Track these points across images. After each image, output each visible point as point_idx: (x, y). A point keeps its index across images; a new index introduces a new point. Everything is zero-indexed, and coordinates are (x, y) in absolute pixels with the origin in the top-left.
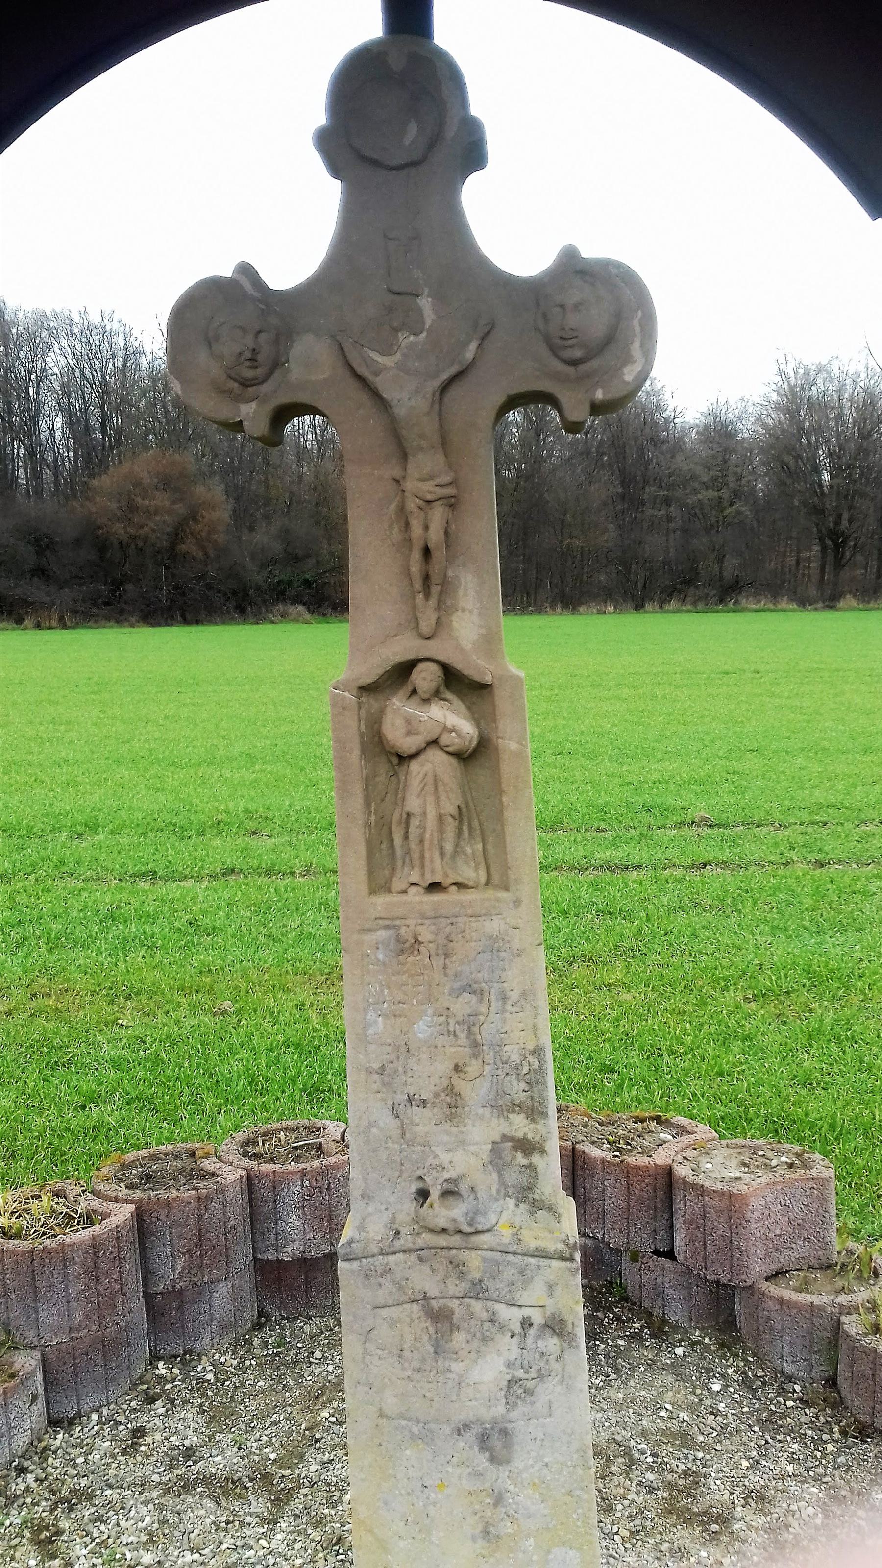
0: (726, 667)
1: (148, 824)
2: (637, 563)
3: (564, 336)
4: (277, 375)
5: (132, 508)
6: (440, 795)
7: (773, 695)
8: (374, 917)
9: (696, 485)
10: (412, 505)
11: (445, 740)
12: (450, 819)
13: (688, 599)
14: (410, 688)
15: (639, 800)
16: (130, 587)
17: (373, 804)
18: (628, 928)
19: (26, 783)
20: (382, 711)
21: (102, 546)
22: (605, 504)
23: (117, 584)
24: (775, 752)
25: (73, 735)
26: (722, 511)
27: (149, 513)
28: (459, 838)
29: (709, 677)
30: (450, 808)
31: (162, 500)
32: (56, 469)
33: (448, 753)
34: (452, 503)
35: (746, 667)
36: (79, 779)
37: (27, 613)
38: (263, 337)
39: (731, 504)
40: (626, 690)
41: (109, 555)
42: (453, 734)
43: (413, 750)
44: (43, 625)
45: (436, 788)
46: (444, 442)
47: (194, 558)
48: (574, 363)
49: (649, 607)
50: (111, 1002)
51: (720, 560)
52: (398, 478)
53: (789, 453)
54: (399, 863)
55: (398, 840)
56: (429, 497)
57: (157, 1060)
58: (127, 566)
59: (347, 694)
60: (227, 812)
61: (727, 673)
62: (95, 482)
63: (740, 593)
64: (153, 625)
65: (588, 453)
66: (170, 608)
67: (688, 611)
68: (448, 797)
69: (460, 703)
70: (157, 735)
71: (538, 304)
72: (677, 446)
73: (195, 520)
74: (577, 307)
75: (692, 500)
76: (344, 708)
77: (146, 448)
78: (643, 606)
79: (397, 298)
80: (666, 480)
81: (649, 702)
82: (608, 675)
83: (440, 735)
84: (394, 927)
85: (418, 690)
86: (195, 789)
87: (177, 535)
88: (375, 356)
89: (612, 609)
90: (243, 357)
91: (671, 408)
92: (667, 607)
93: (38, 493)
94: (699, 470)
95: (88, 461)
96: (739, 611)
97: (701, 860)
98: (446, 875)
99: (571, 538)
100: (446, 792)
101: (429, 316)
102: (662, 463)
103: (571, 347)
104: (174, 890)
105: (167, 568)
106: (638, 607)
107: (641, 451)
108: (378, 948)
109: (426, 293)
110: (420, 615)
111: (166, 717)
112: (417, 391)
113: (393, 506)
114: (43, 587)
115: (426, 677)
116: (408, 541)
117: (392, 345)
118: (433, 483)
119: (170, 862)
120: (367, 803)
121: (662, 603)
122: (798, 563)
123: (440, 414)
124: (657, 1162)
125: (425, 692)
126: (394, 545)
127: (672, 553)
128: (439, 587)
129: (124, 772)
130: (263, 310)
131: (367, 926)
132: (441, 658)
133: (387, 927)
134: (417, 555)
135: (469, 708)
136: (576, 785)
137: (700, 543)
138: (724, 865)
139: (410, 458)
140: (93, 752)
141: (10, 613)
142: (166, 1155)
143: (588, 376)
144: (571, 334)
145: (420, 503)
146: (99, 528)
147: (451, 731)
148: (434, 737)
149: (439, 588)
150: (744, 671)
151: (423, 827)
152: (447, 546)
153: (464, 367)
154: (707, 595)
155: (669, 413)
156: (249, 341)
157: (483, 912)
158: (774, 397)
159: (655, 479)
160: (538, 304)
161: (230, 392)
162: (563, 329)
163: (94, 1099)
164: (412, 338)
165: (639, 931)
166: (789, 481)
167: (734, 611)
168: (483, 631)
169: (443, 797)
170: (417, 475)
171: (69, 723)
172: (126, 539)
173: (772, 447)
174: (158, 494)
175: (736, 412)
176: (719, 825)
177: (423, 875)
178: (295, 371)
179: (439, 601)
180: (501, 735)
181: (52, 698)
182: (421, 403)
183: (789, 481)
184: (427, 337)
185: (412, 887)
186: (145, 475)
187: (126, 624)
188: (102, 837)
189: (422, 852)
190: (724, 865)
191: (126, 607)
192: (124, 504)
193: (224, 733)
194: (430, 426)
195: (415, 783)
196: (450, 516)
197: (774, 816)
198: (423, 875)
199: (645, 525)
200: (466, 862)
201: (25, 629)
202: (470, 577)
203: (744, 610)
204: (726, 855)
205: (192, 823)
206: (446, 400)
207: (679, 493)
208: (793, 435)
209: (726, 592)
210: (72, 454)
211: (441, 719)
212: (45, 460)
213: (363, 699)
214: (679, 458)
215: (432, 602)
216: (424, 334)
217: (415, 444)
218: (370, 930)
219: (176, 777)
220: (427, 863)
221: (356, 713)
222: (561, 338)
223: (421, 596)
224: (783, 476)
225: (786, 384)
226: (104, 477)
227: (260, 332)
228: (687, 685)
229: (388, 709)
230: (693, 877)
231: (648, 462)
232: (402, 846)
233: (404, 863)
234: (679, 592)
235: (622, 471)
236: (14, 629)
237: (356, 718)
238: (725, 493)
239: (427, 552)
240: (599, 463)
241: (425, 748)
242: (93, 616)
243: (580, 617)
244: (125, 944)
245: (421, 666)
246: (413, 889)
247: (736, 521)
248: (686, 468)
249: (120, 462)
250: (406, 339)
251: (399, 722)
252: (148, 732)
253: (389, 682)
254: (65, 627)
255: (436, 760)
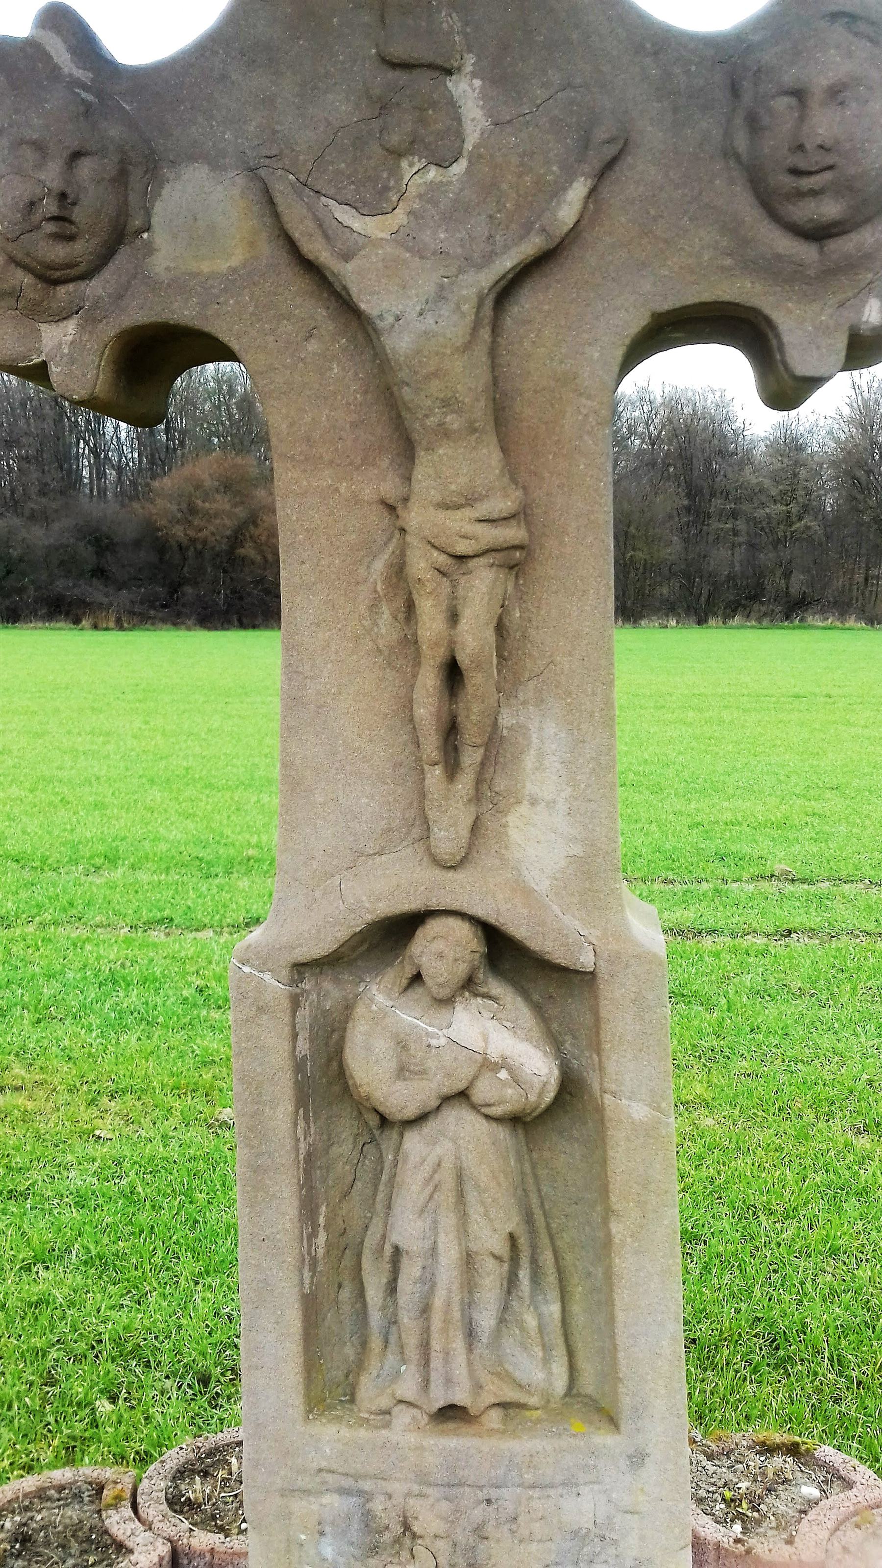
0: (796, 690)
1: (173, 857)
2: (701, 577)
3: (803, 165)
4: (122, 258)
5: (193, 510)
6: (471, 1212)
7: (848, 723)
8: (315, 1466)
9: (764, 498)
10: (420, 564)
11: (483, 1092)
12: (490, 1264)
13: (752, 614)
14: (409, 972)
15: (711, 846)
16: (189, 590)
17: (324, 1208)
18: (706, 1019)
19: (50, 804)
20: (348, 1008)
21: (161, 547)
22: (670, 517)
23: (174, 588)
24: (858, 791)
25: (110, 747)
26: (791, 526)
27: (209, 516)
28: (509, 1292)
29: (778, 703)
30: (490, 1238)
31: (222, 503)
32: (119, 470)
33: (487, 1117)
34: (515, 561)
35: (817, 690)
36: (107, 800)
37: (84, 613)
38: (86, 168)
39: (800, 519)
40: (691, 714)
41: (168, 556)
42: (503, 1074)
43: (411, 1112)
44: (100, 625)
45: (461, 1196)
46: (501, 415)
47: (253, 563)
48: (818, 234)
49: (712, 622)
50: (92, 1103)
51: (787, 575)
52: (391, 501)
53: (861, 467)
54: (376, 1343)
55: (374, 1294)
56: (463, 547)
57: (130, 1195)
58: (186, 569)
59: (267, 977)
60: (258, 846)
61: (797, 696)
62: (156, 484)
63: (806, 610)
64: (209, 629)
65: (654, 465)
66: (227, 612)
67: (752, 627)
68: (486, 1214)
69: (519, 1002)
70: (197, 749)
71: (735, 91)
72: (747, 459)
73: (256, 525)
74: (836, 94)
75: (760, 513)
76: (260, 1010)
77: (211, 450)
78: (706, 621)
79: (401, 77)
80: (734, 493)
81: (715, 727)
82: (671, 695)
83: (475, 1078)
84: (360, 1493)
85: (426, 979)
86: (229, 817)
87: (237, 538)
88: (346, 216)
89: (674, 623)
90: (37, 217)
91: (740, 420)
92: (730, 622)
93: (102, 492)
94: (767, 483)
95: (152, 462)
96: (805, 628)
97: (785, 927)
98: (478, 1387)
99: (634, 549)
100: (482, 1203)
101: (474, 118)
102: (730, 476)
103: (814, 193)
104: (187, 944)
105: (225, 571)
106: (701, 621)
107: (708, 462)
108: (322, 1533)
109: (469, 68)
110: (432, 814)
111: (210, 731)
112: (441, 295)
113: (379, 565)
114: (101, 587)
115: (443, 949)
116: (410, 644)
117: (386, 189)
118: (468, 512)
119: (189, 908)
120: (308, 1210)
121: (726, 618)
122: (866, 580)
123: (493, 353)
124: (803, 1557)
125: (440, 985)
126: (380, 651)
127: (737, 568)
128: (482, 751)
129: (156, 795)
130: (88, 105)
131: (302, 1482)
132: (480, 911)
133: (343, 1492)
134: (429, 679)
135: (538, 1009)
136: (639, 826)
137: (766, 558)
138: (812, 932)
139: (421, 455)
140: (127, 769)
141: (67, 614)
142: (61, 1488)
143: (850, 266)
144: (816, 159)
145: (442, 559)
146: (159, 530)
147: (495, 1067)
148: (461, 1086)
149: (478, 755)
150: (815, 695)
151: (429, 1281)
152: (500, 656)
153: (557, 241)
154: (773, 611)
155: (738, 424)
156: (52, 175)
157: (559, 1478)
158: (846, 411)
159: (722, 493)
160: (735, 91)
161: (16, 294)
162: (801, 147)
163: (45, 1258)
164: (433, 173)
165: (720, 1024)
166: (860, 497)
167: (799, 628)
168: (577, 850)
169: (475, 1213)
170: (435, 496)
171: (108, 734)
172: (185, 542)
173: (844, 460)
174: (218, 497)
175: (807, 425)
176: (804, 881)
177: (426, 1383)
178: (166, 250)
179: (479, 782)
180: (613, 1087)
181: (96, 705)
182: (452, 324)
183: (860, 497)
184: (468, 169)
185: (402, 1407)
186: (205, 476)
187: (183, 627)
188: (120, 871)
189: (426, 1331)
190: (812, 932)
191: (184, 610)
192: (184, 506)
193: (267, 750)
194: (468, 378)
195: (412, 1188)
196: (510, 588)
197: (863, 870)
198: (426, 1383)
199: (711, 538)
200: (524, 1347)
201: (82, 629)
202: (551, 728)
203: (811, 627)
204: (814, 920)
205: (218, 858)
206: (508, 322)
207: (746, 507)
208: (866, 449)
209: (792, 608)
210: (136, 455)
211: (479, 1046)
212: (110, 460)
213: (307, 985)
214: (748, 469)
215: (465, 783)
216: (459, 168)
217: (432, 421)
218: (307, 1492)
219: (210, 800)
220: (436, 1362)
221: (287, 1019)
222: (796, 172)
223: (438, 771)
224: (855, 493)
225: (860, 397)
226: (166, 480)
227: (76, 155)
228: (755, 710)
229: (360, 1010)
230: (777, 947)
231: (716, 473)
232: (384, 1308)
233: (386, 1342)
234: (745, 607)
235: (689, 484)
236: (71, 629)
237: (287, 1029)
238: (794, 508)
239: (453, 674)
240: (666, 474)
241: (438, 1108)
242: (150, 618)
243: (640, 630)
244: (118, 1024)
245: (434, 926)
246: (403, 1417)
247: (805, 536)
248: (755, 481)
249: (183, 464)
250: (417, 175)
251: (382, 1046)
252: (188, 747)
253: (365, 946)
254: (121, 628)
255: (464, 1130)
